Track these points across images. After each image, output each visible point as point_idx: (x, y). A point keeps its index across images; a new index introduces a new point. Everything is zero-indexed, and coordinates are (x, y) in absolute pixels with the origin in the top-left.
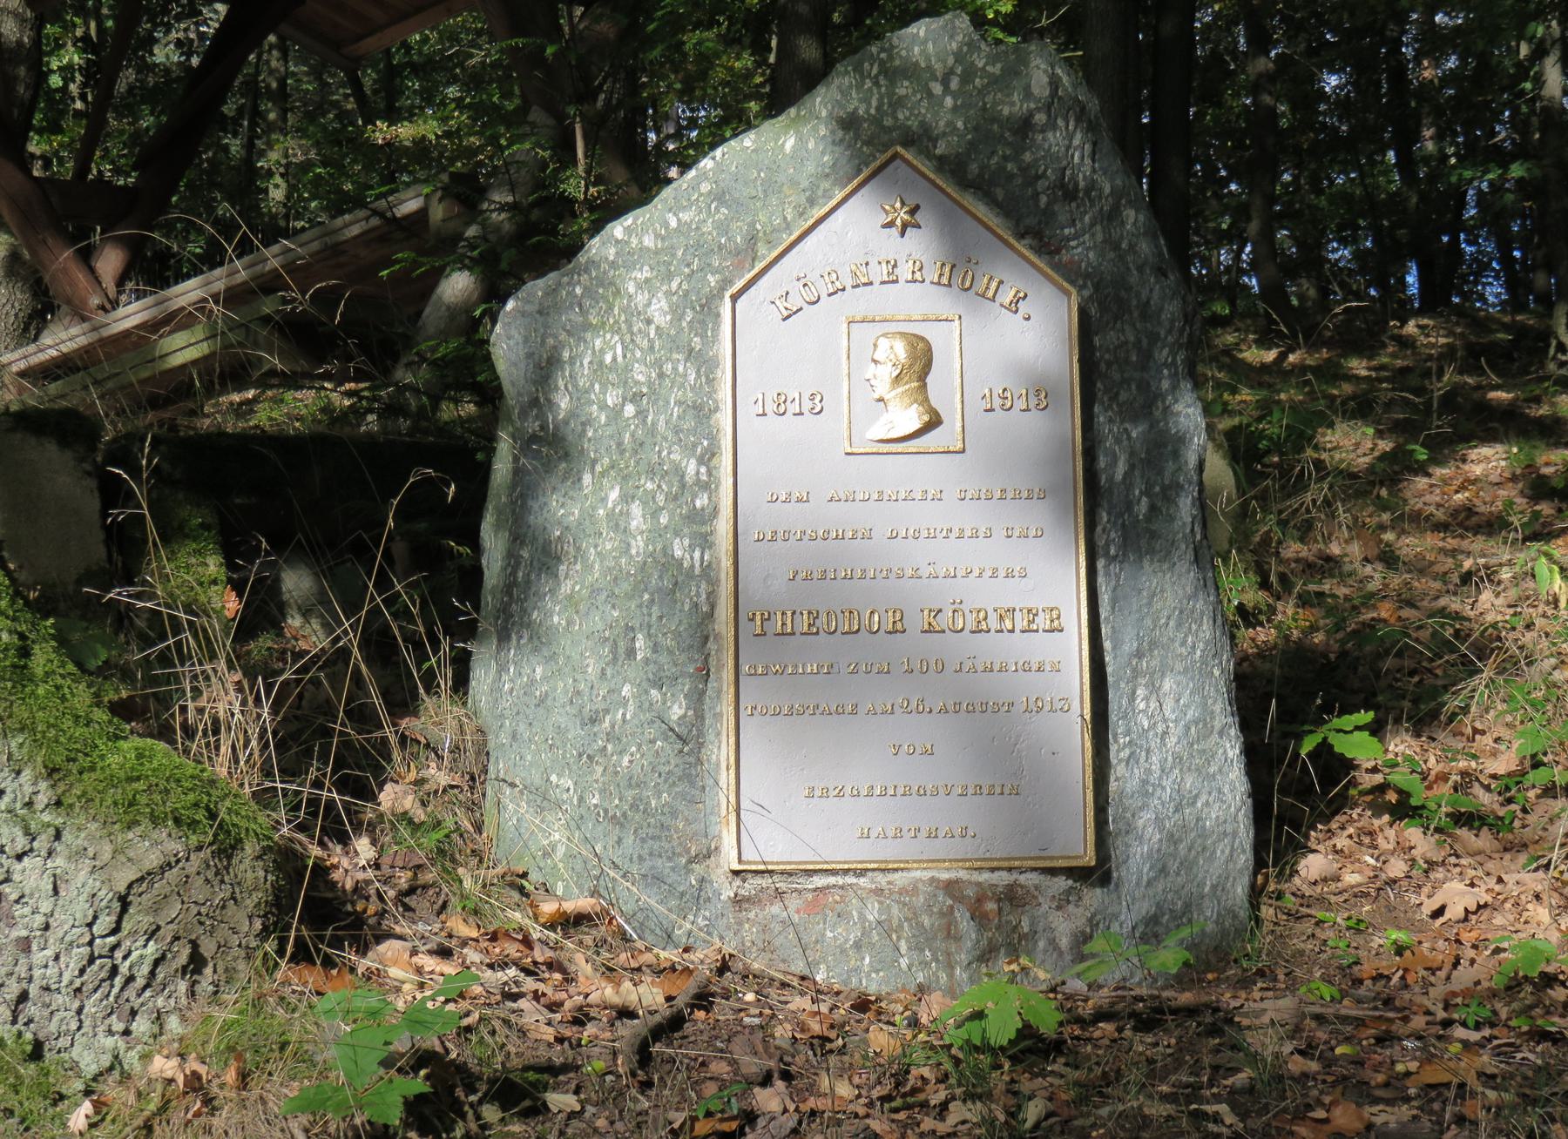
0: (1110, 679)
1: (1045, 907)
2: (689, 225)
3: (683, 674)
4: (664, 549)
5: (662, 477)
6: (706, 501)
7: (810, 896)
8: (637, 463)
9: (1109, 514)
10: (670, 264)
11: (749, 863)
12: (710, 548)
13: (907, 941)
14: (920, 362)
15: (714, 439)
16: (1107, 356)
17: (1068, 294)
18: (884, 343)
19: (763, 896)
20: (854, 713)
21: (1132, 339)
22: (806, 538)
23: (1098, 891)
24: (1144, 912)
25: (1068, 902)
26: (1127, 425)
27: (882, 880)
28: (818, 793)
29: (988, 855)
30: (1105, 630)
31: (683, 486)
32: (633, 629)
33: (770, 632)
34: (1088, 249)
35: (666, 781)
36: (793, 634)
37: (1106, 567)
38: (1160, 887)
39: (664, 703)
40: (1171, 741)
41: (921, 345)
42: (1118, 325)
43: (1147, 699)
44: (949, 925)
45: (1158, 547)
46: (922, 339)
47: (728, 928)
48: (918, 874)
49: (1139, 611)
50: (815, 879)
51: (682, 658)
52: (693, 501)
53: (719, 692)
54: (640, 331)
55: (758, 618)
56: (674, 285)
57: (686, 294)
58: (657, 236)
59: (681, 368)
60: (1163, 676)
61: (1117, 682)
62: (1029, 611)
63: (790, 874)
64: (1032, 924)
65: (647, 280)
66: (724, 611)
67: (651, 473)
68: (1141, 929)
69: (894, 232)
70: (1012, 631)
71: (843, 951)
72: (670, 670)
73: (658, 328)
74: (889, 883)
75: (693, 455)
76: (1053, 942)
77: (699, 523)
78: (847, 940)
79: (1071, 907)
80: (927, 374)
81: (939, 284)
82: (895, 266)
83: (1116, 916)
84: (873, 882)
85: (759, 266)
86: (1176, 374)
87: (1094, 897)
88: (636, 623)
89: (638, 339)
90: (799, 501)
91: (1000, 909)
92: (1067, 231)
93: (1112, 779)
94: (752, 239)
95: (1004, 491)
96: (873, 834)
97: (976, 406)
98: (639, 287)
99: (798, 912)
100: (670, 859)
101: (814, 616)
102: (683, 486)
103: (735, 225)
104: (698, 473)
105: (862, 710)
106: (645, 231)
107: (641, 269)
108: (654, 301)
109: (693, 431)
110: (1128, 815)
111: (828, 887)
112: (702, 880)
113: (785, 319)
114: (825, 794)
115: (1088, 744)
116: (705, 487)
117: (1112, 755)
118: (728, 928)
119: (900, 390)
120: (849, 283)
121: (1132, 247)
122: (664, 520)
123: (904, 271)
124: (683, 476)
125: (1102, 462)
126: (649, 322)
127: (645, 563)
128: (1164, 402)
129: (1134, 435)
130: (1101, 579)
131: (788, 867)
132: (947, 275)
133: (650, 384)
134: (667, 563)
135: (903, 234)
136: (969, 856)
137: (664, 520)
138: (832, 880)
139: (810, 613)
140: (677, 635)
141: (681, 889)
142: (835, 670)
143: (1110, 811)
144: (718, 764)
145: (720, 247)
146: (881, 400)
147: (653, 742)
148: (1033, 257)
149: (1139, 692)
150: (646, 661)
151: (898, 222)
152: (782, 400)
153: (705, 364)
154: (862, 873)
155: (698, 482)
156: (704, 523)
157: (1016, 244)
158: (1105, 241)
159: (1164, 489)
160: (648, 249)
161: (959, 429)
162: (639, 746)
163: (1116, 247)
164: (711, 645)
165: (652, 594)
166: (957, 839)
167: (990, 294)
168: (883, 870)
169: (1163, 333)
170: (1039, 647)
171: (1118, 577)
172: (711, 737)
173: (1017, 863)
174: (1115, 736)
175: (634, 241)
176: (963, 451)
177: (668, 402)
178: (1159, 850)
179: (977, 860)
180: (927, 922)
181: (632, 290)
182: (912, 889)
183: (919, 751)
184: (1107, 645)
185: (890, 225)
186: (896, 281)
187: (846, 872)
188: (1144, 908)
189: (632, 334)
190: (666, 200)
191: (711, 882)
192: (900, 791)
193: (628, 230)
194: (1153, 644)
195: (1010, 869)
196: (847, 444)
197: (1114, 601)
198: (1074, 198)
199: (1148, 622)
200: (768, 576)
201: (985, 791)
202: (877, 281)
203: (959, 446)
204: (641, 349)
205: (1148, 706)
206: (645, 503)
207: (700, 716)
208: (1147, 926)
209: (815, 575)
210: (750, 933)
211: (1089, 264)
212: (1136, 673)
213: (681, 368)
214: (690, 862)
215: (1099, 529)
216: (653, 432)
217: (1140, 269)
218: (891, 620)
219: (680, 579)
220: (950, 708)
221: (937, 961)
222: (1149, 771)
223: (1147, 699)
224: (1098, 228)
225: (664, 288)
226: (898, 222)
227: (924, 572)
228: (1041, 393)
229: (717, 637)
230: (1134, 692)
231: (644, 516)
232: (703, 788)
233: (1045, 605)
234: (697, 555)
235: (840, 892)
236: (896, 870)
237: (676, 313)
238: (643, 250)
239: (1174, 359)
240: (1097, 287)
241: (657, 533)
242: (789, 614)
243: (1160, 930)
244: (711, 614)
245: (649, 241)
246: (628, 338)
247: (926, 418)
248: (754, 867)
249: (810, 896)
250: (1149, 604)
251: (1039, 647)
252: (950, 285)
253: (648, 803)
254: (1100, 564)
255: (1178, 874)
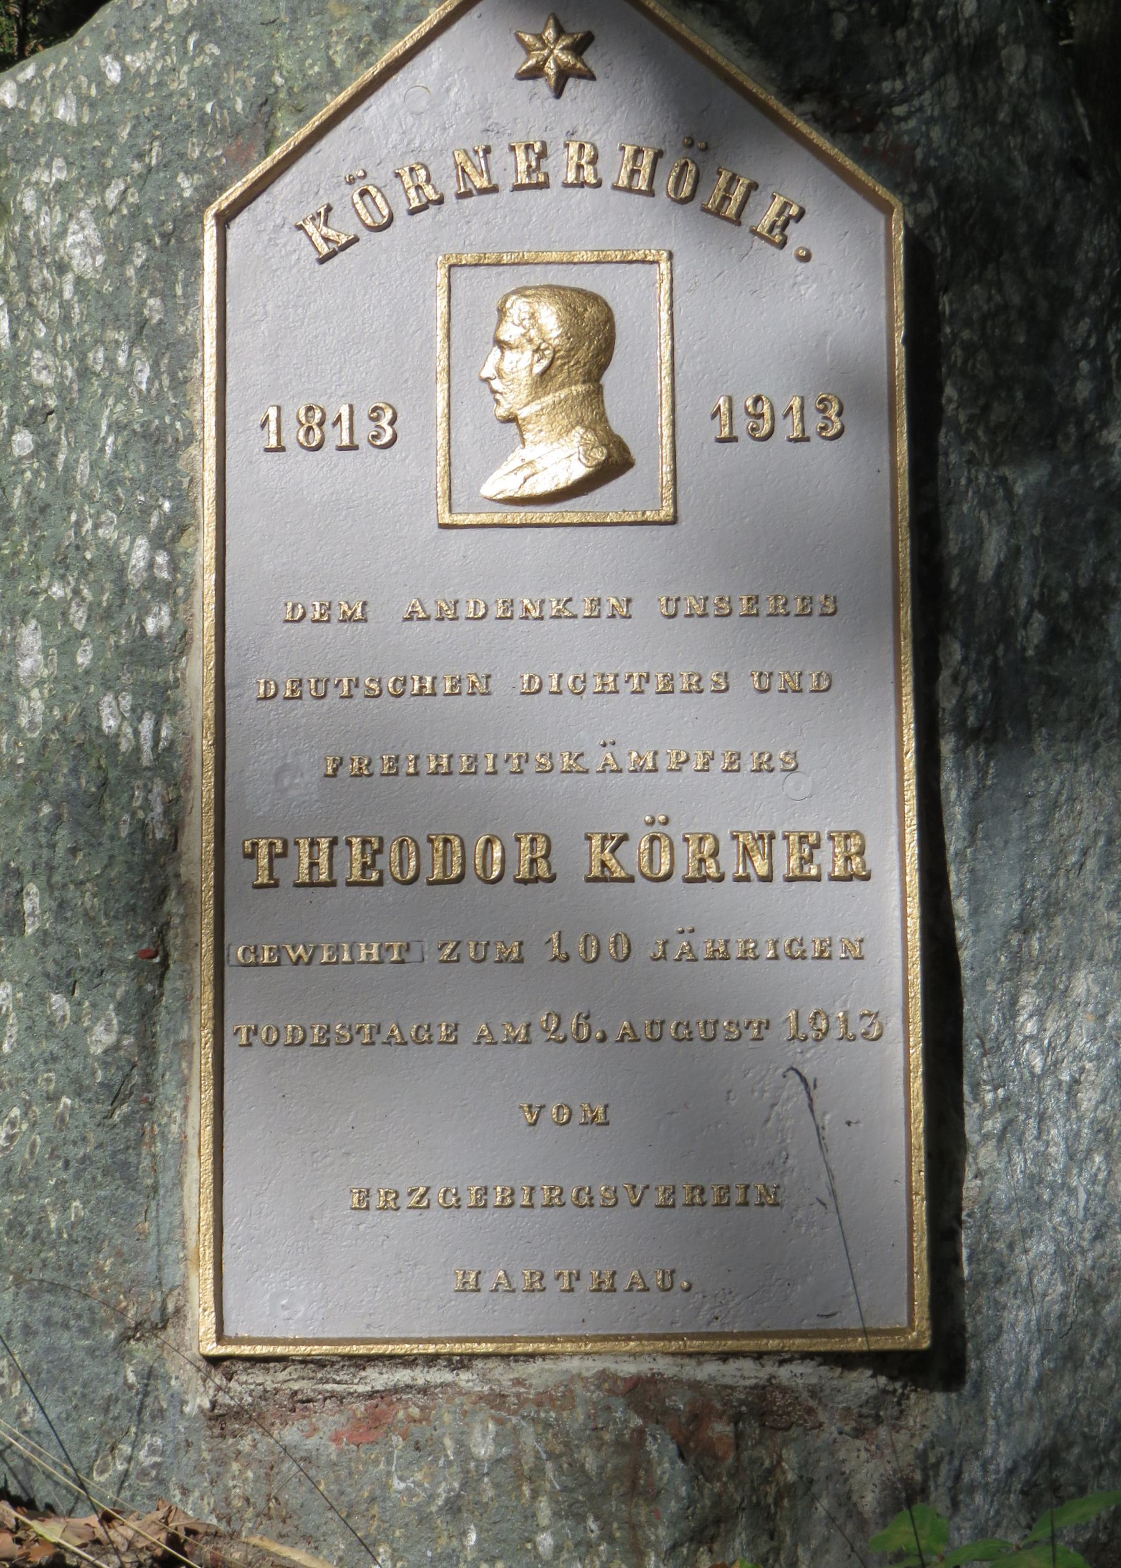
0: (967, 974)
1: (831, 1431)
2: (143, 77)
3: (115, 964)
4: (82, 715)
5: (83, 573)
6: (166, 620)
7: (360, 1408)
8: (35, 545)
9: (965, 646)
10: (105, 153)
11: (239, 1341)
12: (173, 712)
13: (553, 1496)
14: (591, 347)
15: (184, 499)
16: (966, 335)
17: (886, 209)
18: (518, 307)
19: (269, 1408)
20: (451, 1040)
21: (1016, 300)
22: (359, 693)
23: (939, 1398)
24: (1030, 1442)
25: (878, 1420)
26: (1006, 471)
27: (503, 1375)
28: (377, 1201)
29: (715, 1327)
30: (955, 877)
31: (122, 590)
32: (18, 874)
33: (286, 882)
34: (930, 121)
35: (77, 1177)
36: (331, 884)
37: (958, 750)
38: (1065, 1390)
39: (77, 1021)
40: (1087, 1098)
41: (591, 311)
42: (990, 274)
43: (1040, 1013)
44: (635, 1468)
45: (1063, 712)
46: (594, 298)
47: (199, 1469)
48: (574, 1365)
49: (1025, 838)
50: (371, 1373)
51: (113, 931)
52: (141, 621)
53: (187, 998)
54: (44, 287)
55: (263, 851)
56: (112, 196)
57: (136, 212)
58: (83, 100)
59: (122, 360)
60: (1073, 967)
61: (981, 980)
62: (803, 839)
63: (320, 1363)
64: (804, 1465)
65: (60, 186)
66: (199, 840)
67: (62, 565)
68: (1024, 1474)
69: (543, 87)
70: (767, 879)
71: (424, 1519)
72: (88, 955)
73: (79, 280)
74: (518, 1382)
75: (142, 529)
76: (847, 1502)
77: (149, 668)
78: (432, 1497)
79: (883, 1432)
80: (603, 367)
81: (629, 189)
82: (542, 155)
83: (974, 1449)
84: (484, 1379)
85: (278, 153)
86: (1106, 367)
87: (928, 1410)
88: (24, 862)
89: (41, 303)
90: (347, 619)
91: (739, 1436)
92: (886, 86)
93: (969, 1173)
94: (265, 105)
95: (754, 600)
96: (487, 1285)
97: (700, 431)
98: (43, 199)
99: (336, 1439)
100: (84, 1332)
101: (374, 849)
102: (122, 590)
103: (231, 77)
104: (151, 564)
105: (468, 1037)
106: (59, 91)
107: (49, 166)
108: (73, 226)
109: (141, 484)
110: (1001, 1246)
111: (396, 1390)
112: (149, 1375)
113: (322, 260)
114: (392, 1204)
115: (918, 1105)
116: (165, 592)
117: (970, 1125)
118: (199, 1469)
119: (549, 399)
120: (450, 188)
121: (1019, 120)
122: (83, 659)
123: (563, 165)
124: (122, 571)
125: (954, 544)
126: (62, 268)
127: (45, 743)
128: (1079, 424)
129: (1019, 490)
130: (948, 776)
131: (316, 1350)
132: (646, 171)
133: (62, 390)
134: (86, 744)
135: (558, 92)
136: (677, 1329)
137: (83, 659)
138: (403, 1376)
139: (365, 842)
140: (105, 886)
141: (108, 1391)
142: (415, 955)
143: (965, 1238)
144: (182, 1143)
145: (204, 120)
146: (511, 419)
147: (53, 1098)
148: (816, 137)
149: (1023, 1000)
150: (44, 938)
151: (550, 68)
152: (316, 421)
153: (171, 350)
154: (463, 1362)
155: (151, 582)
156: (161, 665)
157: (784, 111)
158: (963, 107)
159: (1078, 597)
160: (63, 125)
161: (667, 478)
162: (27, 1106)
163: (988, 117)
164: (172, 905)
165: (57, 805)
166: (655, 1295)
167: (731, 209)
168: (504, 1357)
169: (1079, 289)
170: (820, 911)
171: (983, 772)
172: (169, 1089)
173: (773, 1344)
174: (976, 1087)
175: (38, 111)
176: (674, 521)
177: (96, 427)
178: (1062, 1316)
179: (693, 1336)
180: (591, 1463)
181: (29, 205)
182: (561, 1397)
183: (579, 1118)
184: (961, 906)
185: (534, 73)
186: (544, 185)
187: (431, 1360)
188: (1032, 1431)
189: (29, 291)
190: (99, 30)
191: (166, 1379)
192: (541, 1198)
193: (26, 90)
194: (1053, 905)
195: (759, 1356)
196: (442, 506)
197: (974, 819)
198: (904, 21)
199: (1043, 861)
200: (284, 768)
201: (711, 1197)
202: (506, 183)
203: (666, 511)
204: (47, 322)
205: (1042, 1029)
206: (47, 626)
207: (148, 1048)
208: (1036, 1468)
209: (376, 768)
210: (242, 1481)
211: (930, 152)
212: (1019, 963)
213: (122, 360)
214: (125, 1338)
215: (945, 676)
216: (65, 484)
217: (1035, 162)
218: (526, 857)
219: (113, 774)
220: (643, 1032)
221: (611, 1540)
222: (1042, 1158)
223: (1040, 1013)
224: (951, 79)
225: (92, 201)
226: (550, 68)
227: (595, 760)
228: (837, 398)
229: (186, 891)
230: (1014, 1001)
231: (44, 651)
232: (155, 1188)
233: (834, 827)
234: (146, 726)
235: (422, 1400)
236: (531, 1356)
237: (116, 250)
238: (56, 126)
239: (1102, 340)
240: (948, 195)
241: (67, 684)
242: (324, 844)
243: (1064, 1476)
244: (173, 845)
245: (65, 111)
246: (21, 300)
247: (599, 455)
248: (246, 1350)
249: (360, 1408)
250: (1045, 826)
251: (820, 911)
252: (650, 193)
253: (43, 1220)
254: (947, 746)
255: (1100, 1364)
